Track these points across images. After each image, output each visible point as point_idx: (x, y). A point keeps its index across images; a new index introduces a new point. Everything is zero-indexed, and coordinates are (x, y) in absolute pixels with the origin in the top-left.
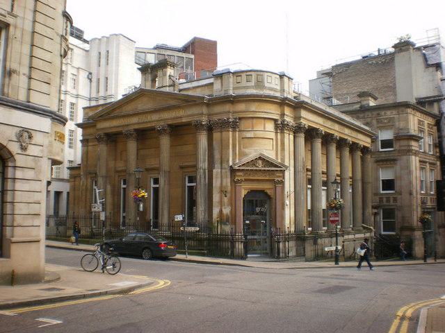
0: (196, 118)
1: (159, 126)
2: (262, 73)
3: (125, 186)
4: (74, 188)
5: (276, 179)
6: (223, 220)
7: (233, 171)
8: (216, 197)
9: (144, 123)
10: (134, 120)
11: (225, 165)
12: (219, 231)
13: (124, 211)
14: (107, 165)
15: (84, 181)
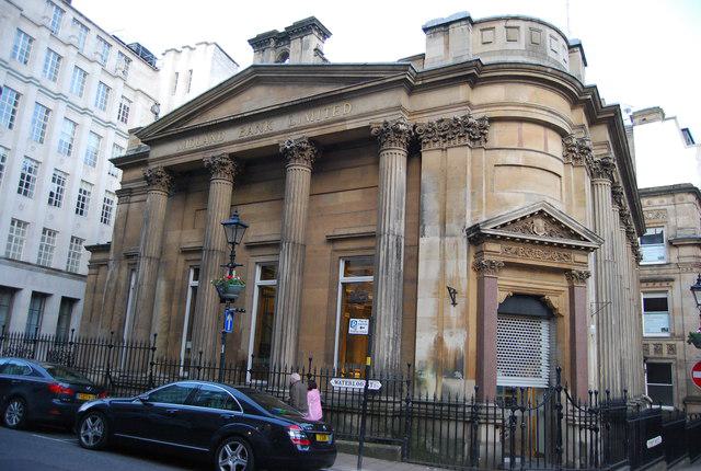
0: (390, 118)
1: (284, 142)
2: (541, 27)
3: (196, 283)
4: (93, 290)
5: (576, 268)
6: (448, 367)
7: (476, 237)
8: (426, 307)
9: (253, 139)
10: (232, 134)
11: (453, 227)
12: (594, 404)
13: (189, 338)
14: (164, 236)
15: (115, 272)
